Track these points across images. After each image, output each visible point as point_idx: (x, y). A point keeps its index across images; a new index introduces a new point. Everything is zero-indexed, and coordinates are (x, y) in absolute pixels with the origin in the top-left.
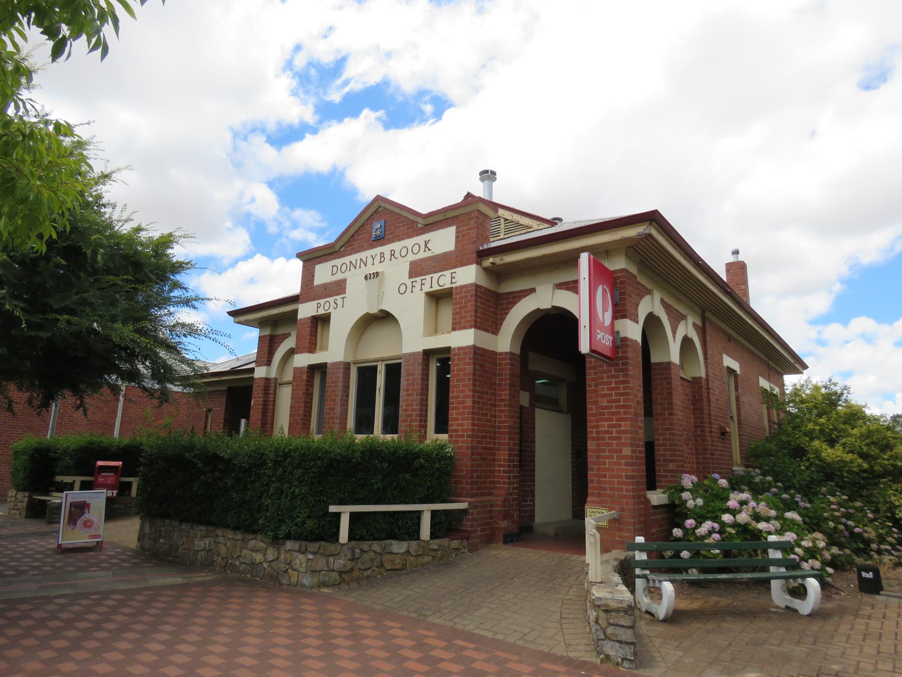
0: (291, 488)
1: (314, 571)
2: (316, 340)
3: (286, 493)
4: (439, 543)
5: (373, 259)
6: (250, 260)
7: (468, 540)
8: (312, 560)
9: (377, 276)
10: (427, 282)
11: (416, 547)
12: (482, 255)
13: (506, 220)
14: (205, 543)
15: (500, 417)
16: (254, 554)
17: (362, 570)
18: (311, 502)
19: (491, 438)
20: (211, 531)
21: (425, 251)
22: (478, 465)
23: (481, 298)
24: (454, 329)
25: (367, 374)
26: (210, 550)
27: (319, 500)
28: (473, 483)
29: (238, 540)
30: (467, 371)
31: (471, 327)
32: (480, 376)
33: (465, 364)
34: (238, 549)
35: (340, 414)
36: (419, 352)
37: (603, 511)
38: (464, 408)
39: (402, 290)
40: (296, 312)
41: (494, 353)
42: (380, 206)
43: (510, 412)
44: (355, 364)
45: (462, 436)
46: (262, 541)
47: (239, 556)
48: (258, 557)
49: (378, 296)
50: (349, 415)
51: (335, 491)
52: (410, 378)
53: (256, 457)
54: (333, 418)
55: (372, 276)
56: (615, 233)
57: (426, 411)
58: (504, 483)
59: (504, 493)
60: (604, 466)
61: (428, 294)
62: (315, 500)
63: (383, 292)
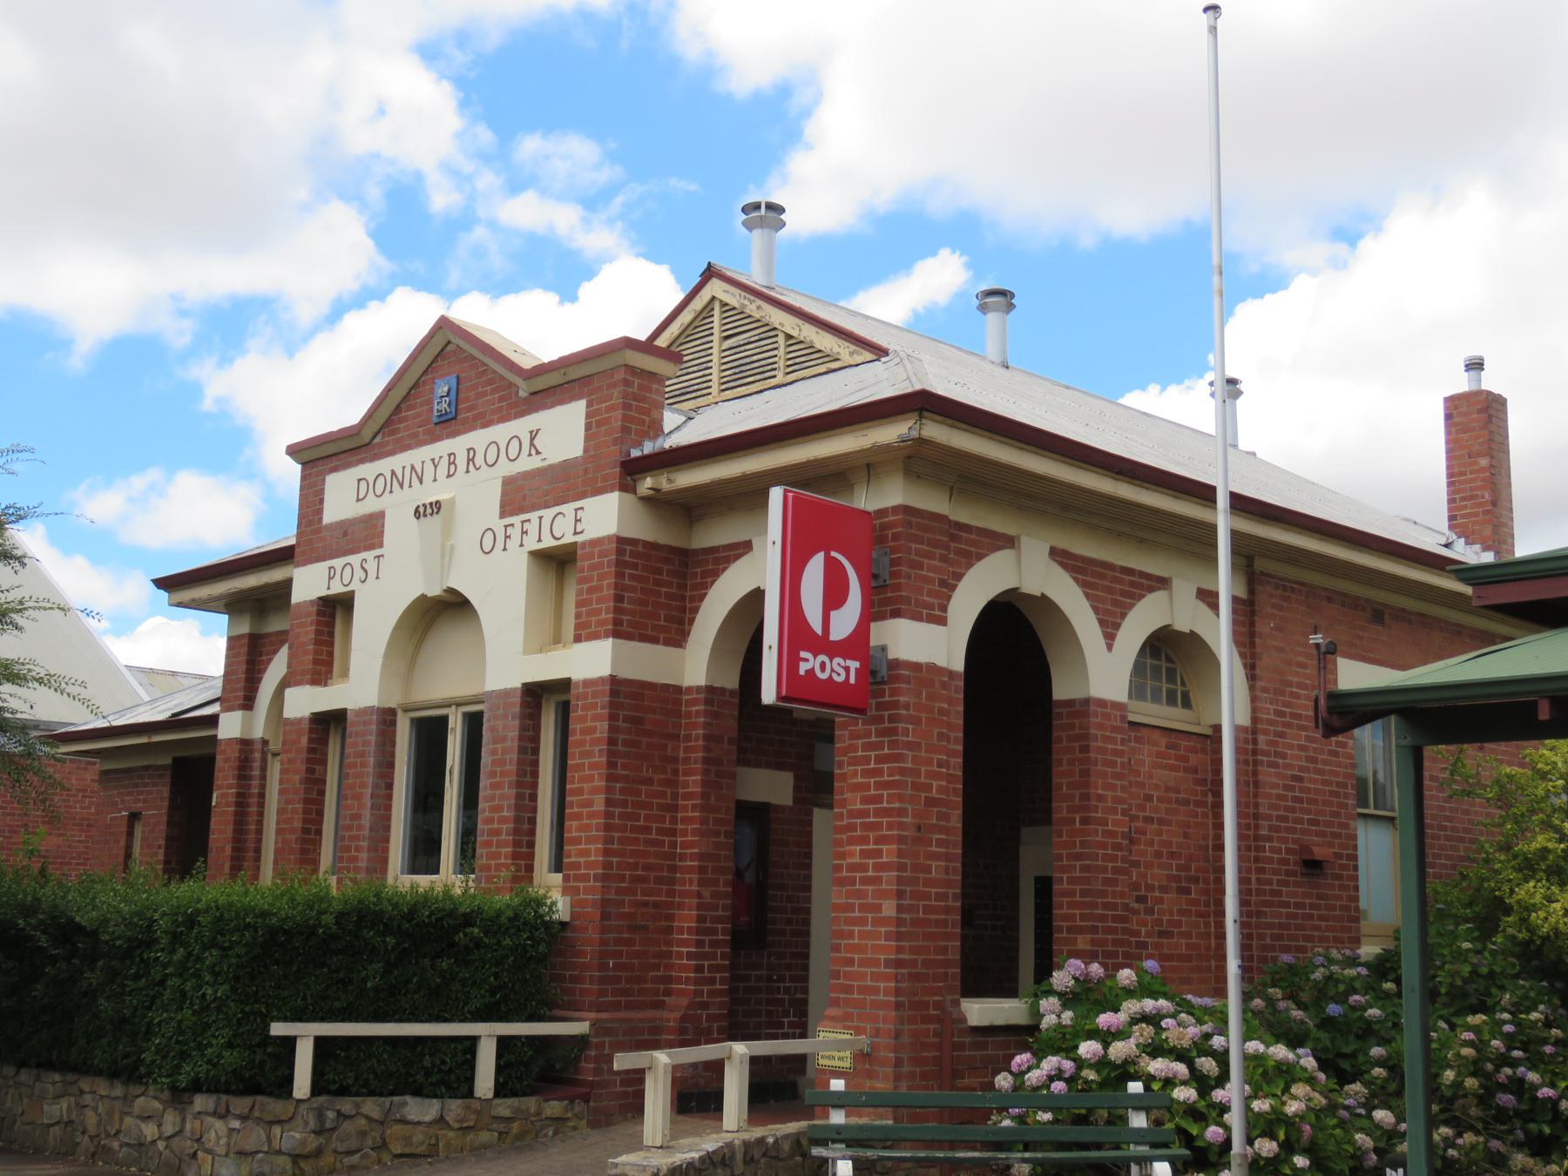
1: (242, 1154)
2: (331, 654)
4: (516, 1105)
5: (436, 467)
6: (374, 305)
7: (587, 1101)
8: (239, 1131)
10: (533, 528)
11: (460, 1111)
12: (632, 470)
13: (789, 337)
14: (61, 1108)
15: (684, 833)
16: (143, 1126)
17: (340, 1153)
18: (235, 1015)
19: (659, 880)
20: (71, 1083)
21: (530, 455)
22: (618, 942)
23: (635, 566)
25: (431, 733)
26: (71, 1122)
28: (602, 980)
29: (118, 1098)
31: (607, 636)
32: (626, 743)
34: (117, 1118)
35: (371, 829)
36: (516, 689)
38: (592, 815)
39: (487, 546)
40: (287, 584)
41: (678, 689)
42: (449, 342)
43: (703, 821)
44: (406, 711)
45: (585, 878)
46: (156, 1098)
47: (118, 1132)
48: (150, 1130)
49: (443, 557)
51: (286, 993)
53: (141, 927)
54: (356, 838)
55: (429, 511)
59: (684, 1001)
60: (851, 942)
61: (534, 554)
62: (243, 1011)
63: (452, 547)
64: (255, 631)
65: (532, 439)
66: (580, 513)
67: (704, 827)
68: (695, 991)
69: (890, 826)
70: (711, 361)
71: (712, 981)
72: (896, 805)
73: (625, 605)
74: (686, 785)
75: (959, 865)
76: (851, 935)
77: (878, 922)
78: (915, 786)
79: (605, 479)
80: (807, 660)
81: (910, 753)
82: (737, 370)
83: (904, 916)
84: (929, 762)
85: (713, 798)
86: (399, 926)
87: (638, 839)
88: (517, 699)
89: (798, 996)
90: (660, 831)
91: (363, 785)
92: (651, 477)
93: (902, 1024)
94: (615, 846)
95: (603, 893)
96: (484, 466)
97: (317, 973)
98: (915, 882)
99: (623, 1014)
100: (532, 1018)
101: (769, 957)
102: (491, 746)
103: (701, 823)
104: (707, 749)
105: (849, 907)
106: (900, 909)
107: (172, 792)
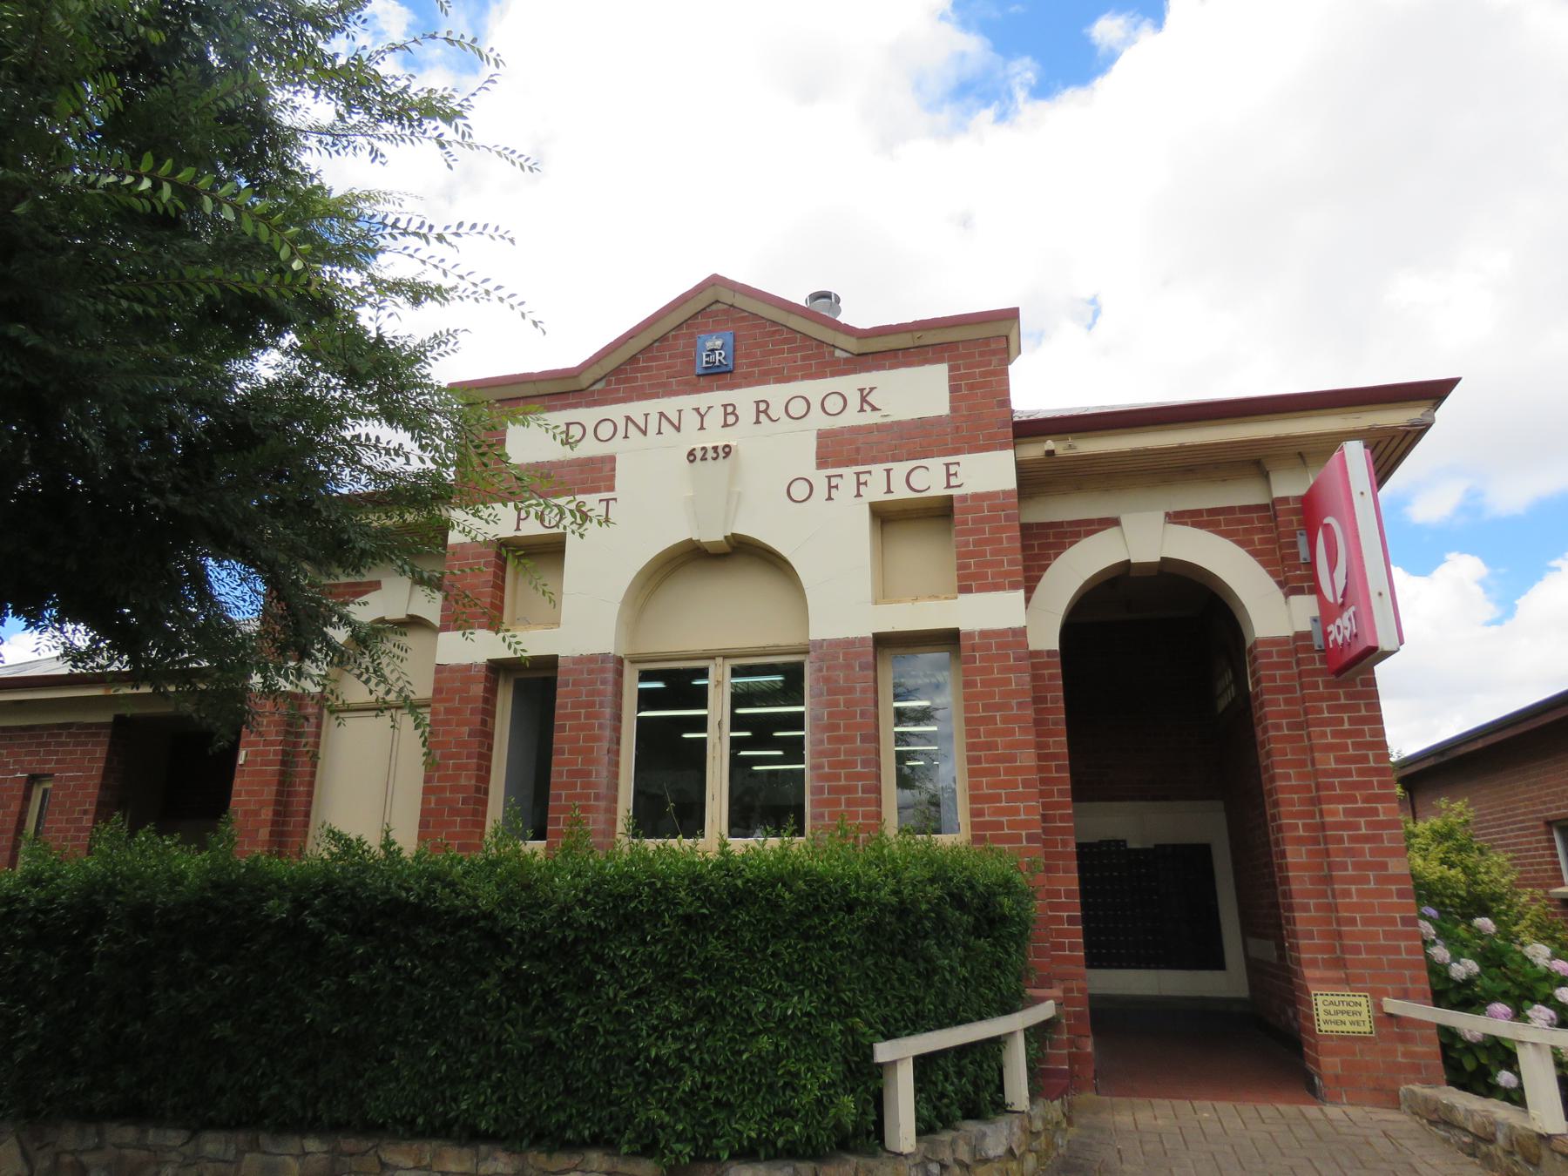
5: (702, 417)
9: (727, 454)
21: (862, 410)
24: (965, 589)
36: (863, 639)
37: (1357, 999)
44: (633, 662)
55: (711, 454)
56: (1357, 415)
92: (1054, 441)
107: (109, 752)
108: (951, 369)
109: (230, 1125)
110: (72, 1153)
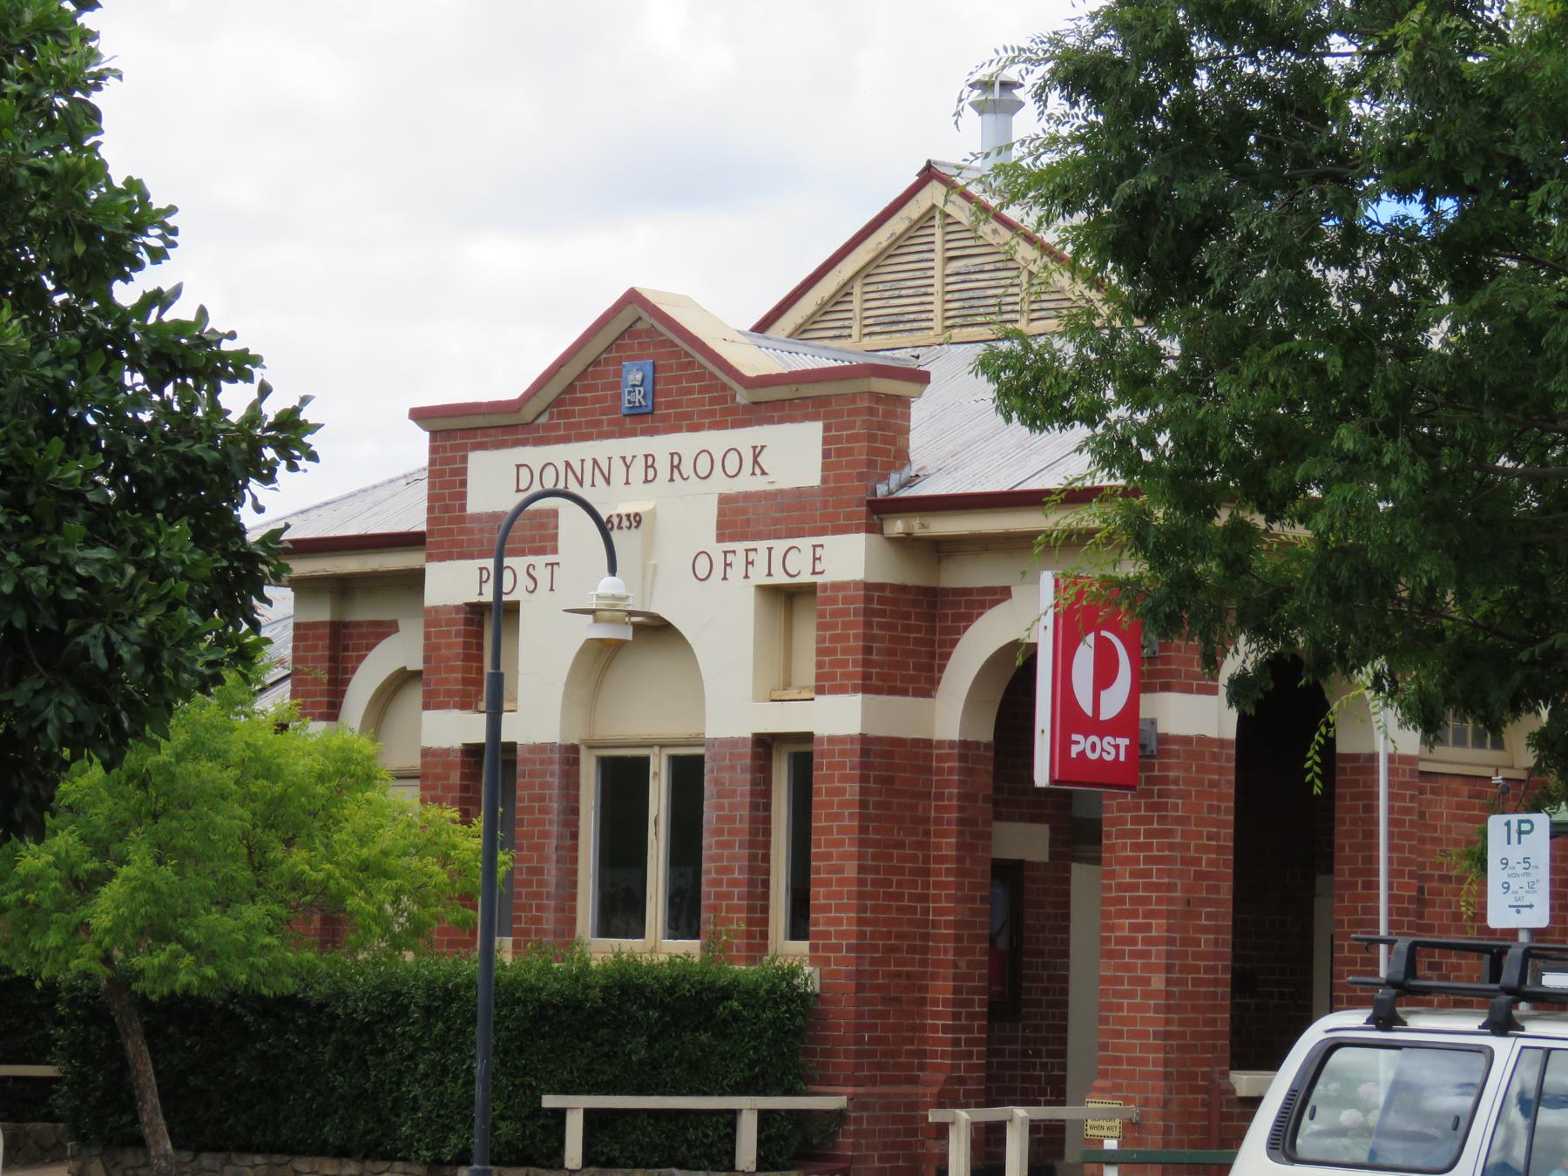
0: (463, 1062)
3: (454, 1073)
5: (628, 467)
9: (639, 523)
10: (760, 558)
15: (937, 899)
19: (912, 949)
21: (753, 474)
23: (882, 613)
24: (820, 690)
27: (522, 1085)
28: (858, 1054)
30: (847, 797)
31: (855, 690)
32: (877, 805)
33: (843, 779)
36: (744, 739)
38: (841, 882)
39: (702, 570)
41: (928, 743)
42: (640, 318)
43: (959, 887)
44: (591, 747)
45: (837, 948)
49: (644, 578)
50: (583, 781)
51: (552, 1067)
52: (726, 801)
53: (383, 1001)
54: (538, 895)
55: (625, 523)
57: (766, 884)
58: (944, 1055)
59: (941, 1076)
62: (513, 1085)
63: (655, 567)
64: (337, 618)
65: (755, 457)
66: (819, 551)
67: (959, 893)
68: (952, 1065)
69: (1160, 901)
70: (932, 285)
71: (969, 1055)
72: (1166, 880)
73: (874, 657)
74: (938, 847)
75: (1229, 937)
76: (1120, 1007)
77: (1147, 995)
78: (1184, 861)
79: (848, 516)
80: (1078, 743)
81: (1180, 828)
82: (967, 304)
83: (1174, 989)
84: (1199, 835)
85: (968, 861)
86: (661, 1000)
87: (890, 907)
88: (748, 750)
89: (1056, 1073)
90: (913, 897)
91: (544, 835)
93: (1171, 1093)
94: (868, 915)
95: (858, 964)
96: (693, 477)
97: (583, 1046)
98: (1184, 955)
99: (880, 1089)
100: (790, 1092)
101: (1024, 1031)
102: (714, 801)
103: (957, 889)
104: (961, 809)
105: (1119, 981)
106: (1168, 982)
108: (827, 428)
109: (218, 1149)
110: (132, 1168)
